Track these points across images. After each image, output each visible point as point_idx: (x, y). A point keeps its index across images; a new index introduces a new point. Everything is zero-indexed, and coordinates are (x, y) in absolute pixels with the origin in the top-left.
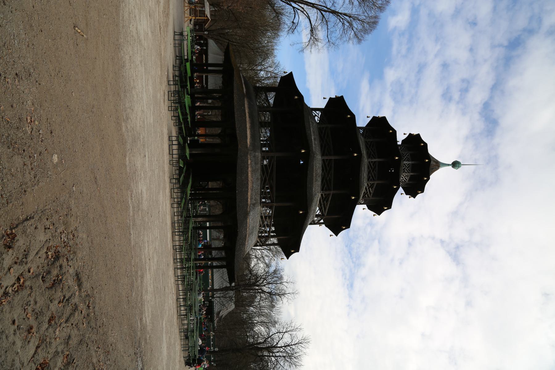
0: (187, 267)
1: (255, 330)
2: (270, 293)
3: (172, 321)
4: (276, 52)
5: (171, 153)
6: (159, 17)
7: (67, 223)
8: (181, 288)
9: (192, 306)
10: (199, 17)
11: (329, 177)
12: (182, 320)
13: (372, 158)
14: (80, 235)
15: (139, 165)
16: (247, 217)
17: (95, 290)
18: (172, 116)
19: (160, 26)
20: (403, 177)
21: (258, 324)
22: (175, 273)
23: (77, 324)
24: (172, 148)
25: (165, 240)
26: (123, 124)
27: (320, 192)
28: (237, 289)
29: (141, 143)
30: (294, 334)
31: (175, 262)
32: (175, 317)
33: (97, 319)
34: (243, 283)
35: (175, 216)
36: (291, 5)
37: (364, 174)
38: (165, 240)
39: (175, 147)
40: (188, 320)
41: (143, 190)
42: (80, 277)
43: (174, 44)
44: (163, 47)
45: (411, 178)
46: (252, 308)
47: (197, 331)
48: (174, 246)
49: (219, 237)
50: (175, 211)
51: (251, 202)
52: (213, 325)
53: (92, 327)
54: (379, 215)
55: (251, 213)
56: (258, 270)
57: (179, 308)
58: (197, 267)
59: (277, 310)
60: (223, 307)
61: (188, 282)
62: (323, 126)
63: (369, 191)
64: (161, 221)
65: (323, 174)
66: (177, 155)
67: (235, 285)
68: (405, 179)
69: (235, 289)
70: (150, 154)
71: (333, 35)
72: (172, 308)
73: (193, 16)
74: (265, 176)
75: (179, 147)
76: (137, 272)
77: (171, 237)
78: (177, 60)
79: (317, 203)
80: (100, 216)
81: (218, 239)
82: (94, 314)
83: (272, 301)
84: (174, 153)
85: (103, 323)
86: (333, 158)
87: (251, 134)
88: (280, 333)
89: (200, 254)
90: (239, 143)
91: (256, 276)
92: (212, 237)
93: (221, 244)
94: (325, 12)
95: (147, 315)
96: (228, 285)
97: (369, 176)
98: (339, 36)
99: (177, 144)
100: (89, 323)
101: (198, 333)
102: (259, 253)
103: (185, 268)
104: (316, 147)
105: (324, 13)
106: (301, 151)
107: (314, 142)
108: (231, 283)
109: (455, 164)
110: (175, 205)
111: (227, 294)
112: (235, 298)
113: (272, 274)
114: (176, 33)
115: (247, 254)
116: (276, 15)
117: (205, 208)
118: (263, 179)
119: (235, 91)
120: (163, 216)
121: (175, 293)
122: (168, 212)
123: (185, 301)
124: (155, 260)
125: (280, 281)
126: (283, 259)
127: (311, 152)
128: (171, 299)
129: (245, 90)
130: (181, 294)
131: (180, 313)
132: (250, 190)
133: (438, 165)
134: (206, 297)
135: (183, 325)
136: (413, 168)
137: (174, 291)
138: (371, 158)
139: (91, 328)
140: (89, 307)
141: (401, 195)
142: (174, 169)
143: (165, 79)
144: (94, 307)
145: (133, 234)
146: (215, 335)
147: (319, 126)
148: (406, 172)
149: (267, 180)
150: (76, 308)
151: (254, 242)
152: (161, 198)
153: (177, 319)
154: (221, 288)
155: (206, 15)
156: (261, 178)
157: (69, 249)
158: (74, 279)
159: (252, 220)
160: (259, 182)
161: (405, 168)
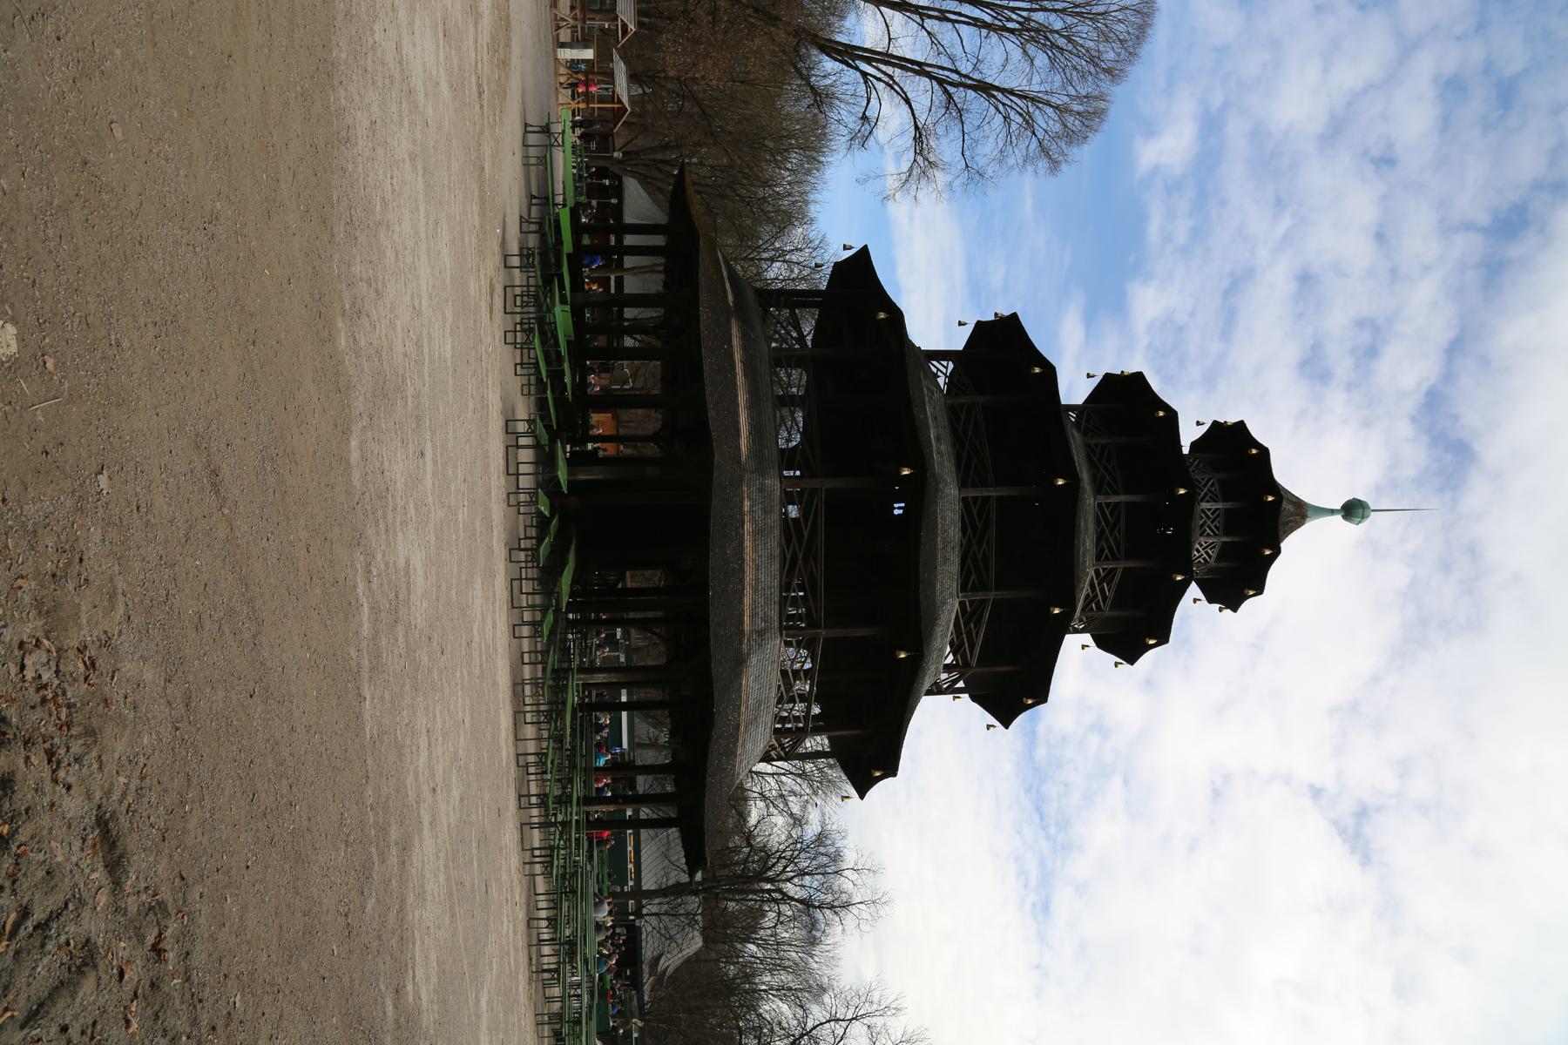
0: (561, 823)
1: (761, 1011)
2: (807, 903)
3: (511, 991)
4: (813, 210)
5: (511, 472)
6: (476, 55)
7: (57, 607)
8: (541, 887)
9: (576, 944)
10: (599, 103)
11: (982, 552)
12: (544, 984)
13: (1107, 494)
14: (128, 668)
15: (398, 473)
16: (742, 671)
17: (197, 887)
18: (516, 365)
19: (479, 85)
20: (1200, 549)
21: (772, 995)
22: (522, 838)
23: (94, 1024)
24: (517, 458)
25: (488, 735)
26: (340, 325)
27: (958, 597)
28: (710, 893)
29: (409, 410)
30: (879, 1024)
31: (522, 806)
32: (521, 977)
33: (200, 1001)
34: (726, 872)
35: (523, 664)
36: (857, 68)
37: (1087, 543)
38: (488, 735)
39: (526, 455)
40: (564, 987)
41: (412, 562)
42: (114, 833)
43: (524, 157)
44: (487, 150)
45: (1225, 552)
46: (752, 947)
47: (591, 1019)
48: (520, 754)
49: (657, 739)
50: (526, 649)
52: (641, 998)
53: (171, 1034)
54: (1132, 664)
55: (754, 660)
56: (770, 835)
57: (534, 949)
58: (591, 824)
59: (827, 951)
60: (669, 945)
61: (564, 867)
62: (963, 401)
63: (1102, 590)
64: (477, 671)
65: (964, 543)
66: (532, 477)
67: (703, 878)
68: (1205, 555)
69: (704, 890)
70: (442, 454)
71: (980, 150)
72: (511, 949)
73: (580, 99)
74: (794, 548)
75: (537, 455)
76: (383, 830)
77: (511, 726)
78: (533, 208)
79: (948, 628)
80: (231, 612)
81: (653, 744)
82: (188, 979)
83: (813, 925)
84: (520, 472)
85: (229, 1014)
86: (993, 493)
88: (837, 1020)
89: (600, 785)
90: (715, 448)
91: (766, 854)
92: (637, 741)
93: (664, 758)
94: (955, 87)
95: (420, 973)
96: (685, 878)
97: (1100, 546)
98: (995, 153)
99: (531, 472)
100: (157, 1017)
101: (594, 1024)
102: (773, 784)
103: (554, 824)
104: (943, 461)
105: (951, 89)
106: (898, 473)
107: (938, 448)
108: (692, 875)
109: (1353, 510)
110: (526, 631)
111: (680, 905)
112: (703, 917)
113: (812, 846)
114: (530, 129)
115: (737, 788)
116: (815, 100)
117: (616, 654)
118: (788, 556)
119: (703, 296)
120: (484, 657)
121: (524, 900)
122: (500, 650)
123: (555, 928)
124: (456, 793)
125: (833, 867)
126: (848, 797)
127: (928, 475)
128: (509, 921)
129: (730, 298)
130: (542, 905)
131: (539, 963)
132: (748, 591)
133: (1300, 512)
134: (619, 913)
135: (549, 1000)
136: (1230, 523)
137: (519, 896)
138: (1105, 494)
139: (168, 1038)
140: (157, 950)
141: (1195, 602)
142: (521, 522)
143: (495, 246)
144: (188, 954)
145: (373, 698)
146: (646, 1027)
147: (949, 401)
148: (1208, 535)
149: (800, 562)
150: (88, 961)
151: (761, 747)
152: (478, 602)
153: (529, 984)
154: (664, 886)
155: (618, 96)
156: (780, 554)
157: (63, 717)
158: (84, 840)
159: (756, 679)
160: (777, 566)
161: (1205, 522)
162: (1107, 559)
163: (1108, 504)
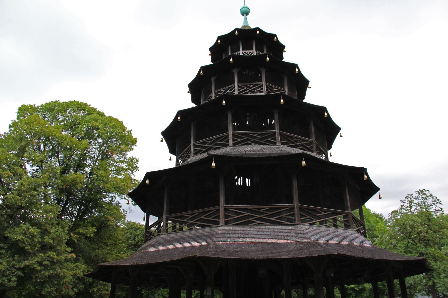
51: (292, 239)
65: (254, 144)
86: (230, 133)
87: (192, 241)
109: (245, 12)
118: (259, 222)
132: (274, 241)
162: (262, 89)
163: (239, 90)
